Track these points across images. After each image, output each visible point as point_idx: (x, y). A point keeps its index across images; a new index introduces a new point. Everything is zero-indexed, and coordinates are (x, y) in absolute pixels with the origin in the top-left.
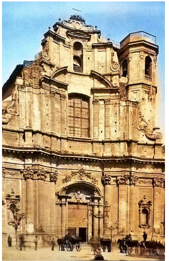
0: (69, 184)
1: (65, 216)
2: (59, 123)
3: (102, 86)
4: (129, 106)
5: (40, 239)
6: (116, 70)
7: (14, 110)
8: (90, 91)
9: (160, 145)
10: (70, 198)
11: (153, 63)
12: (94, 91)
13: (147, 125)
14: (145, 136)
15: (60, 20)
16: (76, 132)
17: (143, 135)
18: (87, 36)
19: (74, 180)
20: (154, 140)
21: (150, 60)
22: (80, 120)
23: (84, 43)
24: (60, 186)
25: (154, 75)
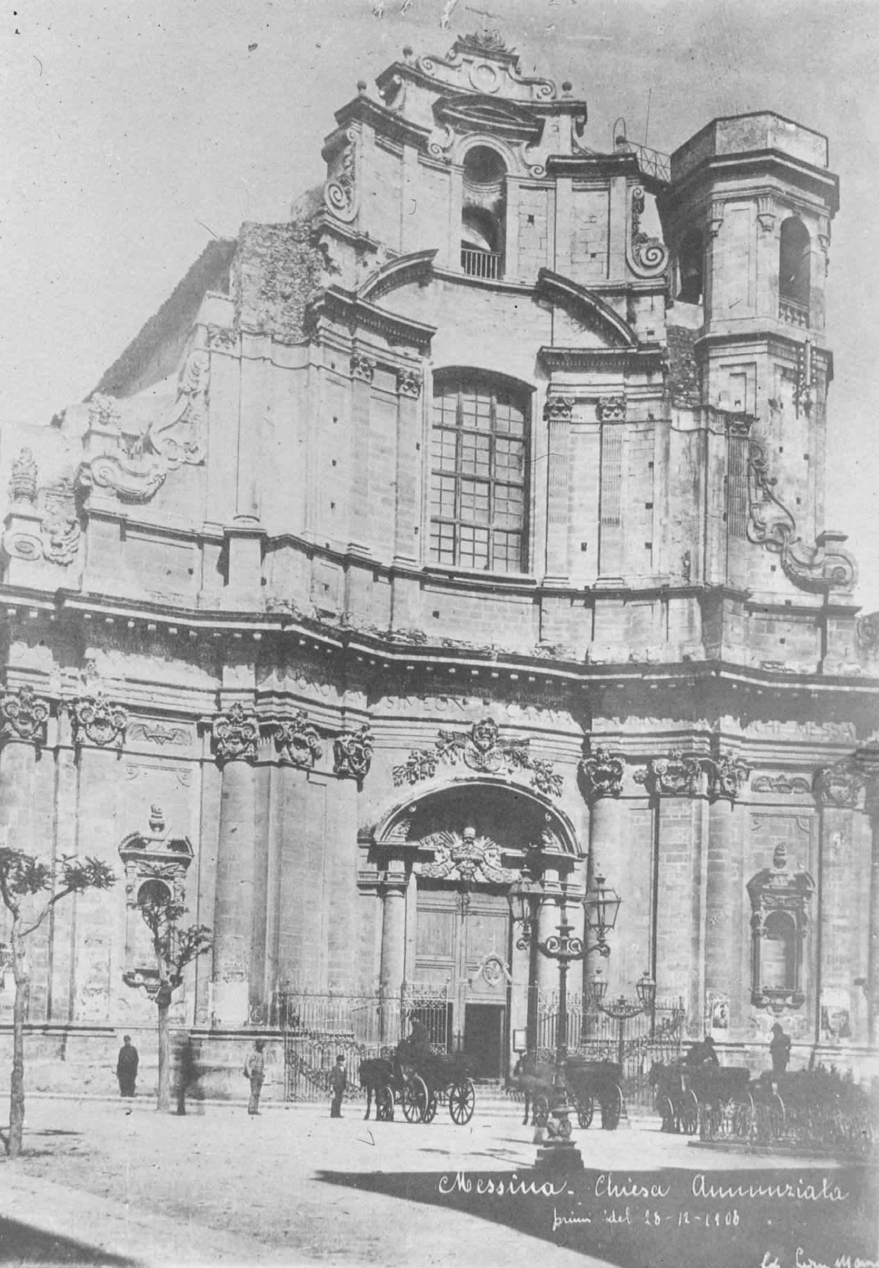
8: (532, 363)
12: (549, 361)
14: (780, 571)
18: (527, 122)
19: (449, 774)
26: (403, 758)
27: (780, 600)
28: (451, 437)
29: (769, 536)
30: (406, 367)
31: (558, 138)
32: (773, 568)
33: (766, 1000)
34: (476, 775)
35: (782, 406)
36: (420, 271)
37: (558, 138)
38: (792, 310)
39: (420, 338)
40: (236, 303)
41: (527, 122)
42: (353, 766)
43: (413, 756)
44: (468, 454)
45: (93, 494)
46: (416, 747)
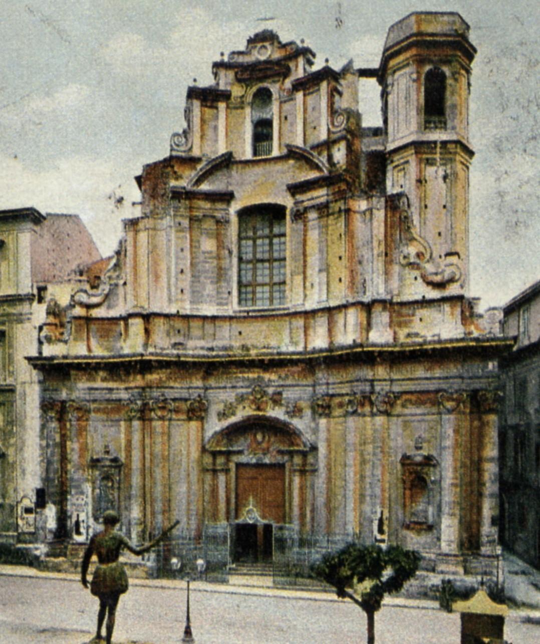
0: (233, 420)
1: (296, 511)
2: (212, 282)
3: (313, 175)
4: (374, 211)
5: (416, 635)
6: (339, 129)
7: (117, 273)
8: (41, 305)
9: (461, 298)
10: (240, 452)
11: (449, 81)
12: (295, 189)
13: (423, 251)
14: (420, 280)
15: (195, 80)
16: (259, 295)
17: (416, 278)
18: (279, 69)
19: (243, 413)
20: (441, 285)
21: (443, 77)
22: (267, 265)
23: (274, 88)
24: (215, 425)
25: (181, 234)
26: (221, 407)
27: (419, 297)
28: (259, 242)
29: (412, 260)
30: (218, 215)
31: (299, 70)
32: (416, 278)
33: (412, 526)
34: (255, 413)
35: (426, 181)
36: (226, 162)
37: (299, 70)
38: (435, 123)
39: (227, 197)
40: (198, 537)
41: (279, 69)
42: (197, 411)
43: (225, 406)
44: (259, 249)
45: (287, 142)
46: (228, 401)
